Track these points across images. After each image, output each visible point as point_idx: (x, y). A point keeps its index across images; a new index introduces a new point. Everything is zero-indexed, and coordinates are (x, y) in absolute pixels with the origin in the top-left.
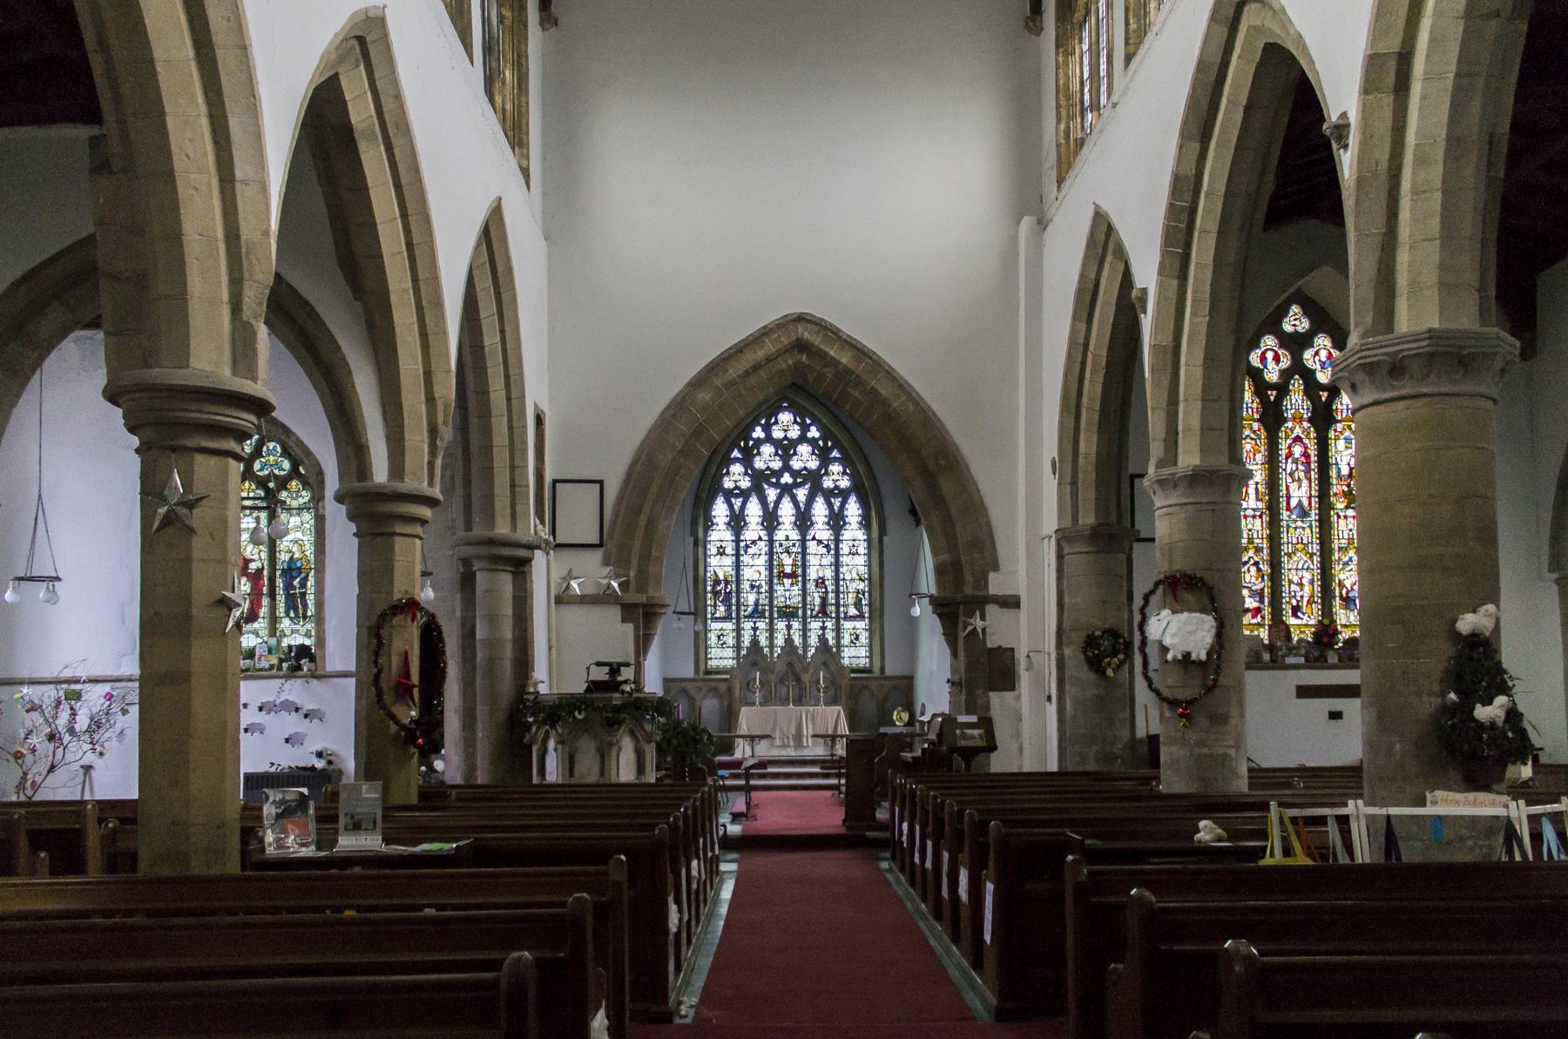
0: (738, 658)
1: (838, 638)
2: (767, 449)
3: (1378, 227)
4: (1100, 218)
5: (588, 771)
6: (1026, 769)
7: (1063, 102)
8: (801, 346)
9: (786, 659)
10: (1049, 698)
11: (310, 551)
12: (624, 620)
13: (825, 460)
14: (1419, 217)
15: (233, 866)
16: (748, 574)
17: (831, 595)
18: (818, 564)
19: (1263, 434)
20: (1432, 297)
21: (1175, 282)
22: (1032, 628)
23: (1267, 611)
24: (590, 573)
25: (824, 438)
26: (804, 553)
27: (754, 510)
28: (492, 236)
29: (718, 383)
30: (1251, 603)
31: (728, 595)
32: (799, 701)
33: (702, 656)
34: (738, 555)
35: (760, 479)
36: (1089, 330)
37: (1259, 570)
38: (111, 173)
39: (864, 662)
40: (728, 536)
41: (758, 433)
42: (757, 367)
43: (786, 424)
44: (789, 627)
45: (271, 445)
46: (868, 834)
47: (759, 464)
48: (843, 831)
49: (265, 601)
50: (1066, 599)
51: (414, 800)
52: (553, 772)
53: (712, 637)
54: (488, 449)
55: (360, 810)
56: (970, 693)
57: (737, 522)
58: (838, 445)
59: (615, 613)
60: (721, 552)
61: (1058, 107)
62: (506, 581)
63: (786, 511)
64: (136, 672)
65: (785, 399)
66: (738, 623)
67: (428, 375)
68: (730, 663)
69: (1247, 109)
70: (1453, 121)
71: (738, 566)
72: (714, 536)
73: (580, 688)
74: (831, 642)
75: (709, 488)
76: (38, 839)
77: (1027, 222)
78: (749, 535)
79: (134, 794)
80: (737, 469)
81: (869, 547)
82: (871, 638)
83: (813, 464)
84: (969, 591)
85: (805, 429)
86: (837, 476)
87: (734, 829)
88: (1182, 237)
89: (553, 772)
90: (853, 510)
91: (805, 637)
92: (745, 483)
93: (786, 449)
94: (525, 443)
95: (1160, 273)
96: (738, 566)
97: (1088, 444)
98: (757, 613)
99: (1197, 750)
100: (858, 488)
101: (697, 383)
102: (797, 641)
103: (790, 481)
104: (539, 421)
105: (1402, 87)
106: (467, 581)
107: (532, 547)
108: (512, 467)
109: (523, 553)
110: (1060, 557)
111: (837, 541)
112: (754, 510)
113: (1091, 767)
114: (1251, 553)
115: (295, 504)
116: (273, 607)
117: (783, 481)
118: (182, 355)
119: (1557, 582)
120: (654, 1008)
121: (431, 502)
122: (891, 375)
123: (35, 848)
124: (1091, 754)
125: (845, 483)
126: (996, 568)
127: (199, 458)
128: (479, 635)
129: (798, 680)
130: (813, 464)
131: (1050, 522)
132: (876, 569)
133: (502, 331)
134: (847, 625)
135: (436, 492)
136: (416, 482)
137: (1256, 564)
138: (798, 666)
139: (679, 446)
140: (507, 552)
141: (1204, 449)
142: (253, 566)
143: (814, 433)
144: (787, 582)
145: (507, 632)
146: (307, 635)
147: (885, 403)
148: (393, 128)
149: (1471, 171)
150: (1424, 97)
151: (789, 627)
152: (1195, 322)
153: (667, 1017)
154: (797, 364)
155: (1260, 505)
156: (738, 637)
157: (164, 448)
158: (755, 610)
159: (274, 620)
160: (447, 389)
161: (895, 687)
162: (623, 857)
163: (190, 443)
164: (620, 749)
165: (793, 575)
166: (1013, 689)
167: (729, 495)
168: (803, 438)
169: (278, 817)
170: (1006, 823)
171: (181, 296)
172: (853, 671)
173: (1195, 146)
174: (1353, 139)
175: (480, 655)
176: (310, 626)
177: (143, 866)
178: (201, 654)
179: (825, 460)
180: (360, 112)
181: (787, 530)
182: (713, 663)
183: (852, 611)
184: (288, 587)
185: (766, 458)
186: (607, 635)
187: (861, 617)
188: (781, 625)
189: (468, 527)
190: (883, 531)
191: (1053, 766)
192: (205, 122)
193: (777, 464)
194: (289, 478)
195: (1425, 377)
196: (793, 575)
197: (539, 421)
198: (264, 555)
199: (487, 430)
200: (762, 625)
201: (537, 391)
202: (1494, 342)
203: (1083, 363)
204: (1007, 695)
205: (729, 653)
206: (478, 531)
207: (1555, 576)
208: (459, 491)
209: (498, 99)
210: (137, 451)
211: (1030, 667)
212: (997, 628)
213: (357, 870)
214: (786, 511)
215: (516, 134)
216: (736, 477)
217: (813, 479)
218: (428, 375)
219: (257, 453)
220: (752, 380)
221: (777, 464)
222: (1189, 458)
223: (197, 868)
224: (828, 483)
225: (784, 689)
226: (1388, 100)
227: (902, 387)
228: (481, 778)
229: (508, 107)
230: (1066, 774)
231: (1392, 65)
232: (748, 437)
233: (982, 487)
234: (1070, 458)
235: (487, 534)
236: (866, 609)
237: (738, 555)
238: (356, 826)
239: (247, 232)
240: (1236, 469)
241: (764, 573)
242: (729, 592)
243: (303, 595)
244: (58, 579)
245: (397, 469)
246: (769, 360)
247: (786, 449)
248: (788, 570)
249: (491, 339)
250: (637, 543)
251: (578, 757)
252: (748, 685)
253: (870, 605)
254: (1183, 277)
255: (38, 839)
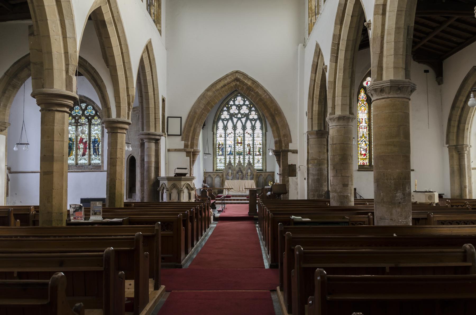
0: (225, 166)
1: (253, 161)
2: (234, 107)
3: (378, 50)
4: (317, 45)
5: (175, 198)
6: (299, 199)
7: (310, 12)
8: (237, 80)
9: (239, 167)
10: (305, 179)
11: (100, 137)
12: (187, 156)
13: (250, 110)
14: (389, 49)
15: (64, 225)
16: (228, 142)
17: (252, 149)
18: (248, 140)
19: (367, 105)
20: (392, 71)
21: (334, 64)
22: (300, 160)
23: (368, 155)
24: (179, 143)
25: (250, 104)
26: (244, 137)
27: (230, 125)
28: (148, 49)
29: (214, 90)
30: (363, 152)
31: (223, 149)
32: (242, 179)
33: (215, 166)
34: (225, 137)
35: (232, 116)
36: (315, 76)
37: (366, 143)
38: (34, 35)
39: (261, 168)
40: (223, 132)
41: (231, 103)
42: (225, 86)
43: (239, 100)
44: (239, 158)
45: (90, 106)
46: (255, 216)
47: (232, 111)
48: (248, 216)
49: (88, 150)
50: (310, 151)
51: (123, 206)
52: (165, 199)
53: (218, 160)
54: (148, 108)
55: (96, 209)
56: (284, 177)
57: (225, 128)
58: (254, 106)
59: (184, 154)
60: (221, 136)
61: (309, 13)
62: (153, 145)
63: (239, 125)
64: (39, 170)
65: (239, 93)
66: (225, 157)
67: (127, 88)
68: (223, 168)
69: (352, 17)
70: (397, 23)
71: (225, 140)
72: (218, 132)
73: (172, 175)
74: (251, 162)
75: (217, 119)
76: (17, 216)
77: (301, 45)
78: (228, 132)
79: (39, 205)
80: (225, 113)
81: (263, 135)
82: (263, 161)
83: (247, 111)
84: (283, 148)
85: (245, 101)
86: (253, 115)
87: (218, 215)
88: (336, 52)
89: (165, 199)
90: (258, 124)
91: (244, 160)
92: (228, 117)
93: (239, 107)
94: (159, 107)
95: (330, 61)
96: (225, 140)
97: (316, 108)
98: (231, 154)
99: (339, 194)
100: (259, 118)
101: (208, 90)
102: (242, 162)
103: (240, 116)
104: (163, 100)
105: (384, 13)
106: (142, 145)
107: (160, 136)
108: (155, 113)
109: (158, 137)
110: (308, 139)
111: (253, 133)
112: (230, 125)
113: (316, 198)
114: (363, 138)
115: (96, 123)
116: (90, 152)
117: (238, 116)
118: (52, 86)
119: (448, 147)
120: (177, 264)
121: (129, 124)
122: (262, 88)
123: (16, 219)
124: (316, 195)
125: (256, 117)
126: (291, 142)
127: (56, 113)
128: (145, 160)
129: (242, 173)
130: (247, 111)
131: (306, 130)
132: (264, 141)
133: (152, 76)
134: (256, 157)
135: (130, 121)
136: (124, 118)
137: (365, 141)
138: (242, 169)
139: (203, 107)
140: (153, 137)
141: (342, 110)
142: (84, 140)
143: (247, 103)
144: (239, 145)
145: (153, 159)
146: (99, 160)
147: (260, 96)
148: (117, 21)
149: (401, 37)
150: (389, 17)
151: (239, 158)
152: (340, 75)
153: (181, 267)
154: (236, 85)
155: (366, 125)
156: (225, 160)
157: (46, 110)
158: (230, 153)
159: (90, 155)
160: (134, 91)
161: (269, 175)
162: (159, 223)
163: (54, 109)
164: (184, 192)
165: (241, 143)
166: (296, 176)
167: (223, 120)
168: (244, 104)
169: (74, 212)
170: (274, 214)
171: (51, 69)
172: (257, 170)
173: (339, 26)
174: (372, 27)
175: (145, 166)
176: (100, 157)
177: (40, 225)
178: (56, 167)
179: (250, 110)
180: (107, 17)
181: (239, 130)
182: (218, 168)
183: (258, 153)
184: (94, 146)
185: (234, 110)
186: (181, 160)
187: (260, 155)
188: (237, 157)
189: (143, 130)
190: (266, 131)
191: (306, 198)
192: (58, 22)
193: (237, 112)
194: (94, 116)
195: (389, 93)
196: (241, 143)
197: (163, 100)
198: (87, 137)
199: (148, 103)
200: (232, 157)
201: (162, 92)
202: (408, 83)
203: (314, 85)
204: (294, 178)
205: (223, 165)
206: (145, 131)
207: (448, 145)
208: (140, 120)
209: (152, 11)
210: (40, 111)
211: (300, 170)
212: (292, 159)
213: (96, 226)
214: (239, 125)
215: (157, 21)
216: (225, 115)
217: (247, 116)
218: (127, 88)
219: (86, 109)
220: (223, 89)
221: (237, 112)
222: (338, 112)
223: (54, 224)
224: (251, 117)
225: (238, 175)
226: (380, 17)
227: (265, 91)
228: (146, 200)
229: (155, 13)
230: (309, 200)
231: (381, 7)
232: (228, 104)
233: (287, 120)
234: (311, 112)
235: (148, 132)
236: (261, 153)
237: (225, 137)
238: (95, 214)
239: (70, 51)
240: (351, 116)
241: (233, 142)
242: (223, 148)
243: (98, 148)
244: (28, 144)
245: (119, 115)
246: (228, 84)
247: (239, 107)
248: (240, 141)
249: (149, 78)
250: (191, 135)
251: (172, 195)
252: (228, 174)
253: (263, 152)
254: (336, 62)
255: (17, 216)
